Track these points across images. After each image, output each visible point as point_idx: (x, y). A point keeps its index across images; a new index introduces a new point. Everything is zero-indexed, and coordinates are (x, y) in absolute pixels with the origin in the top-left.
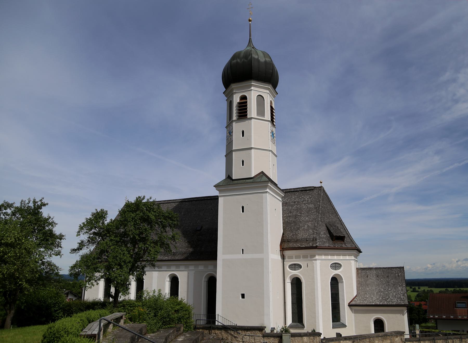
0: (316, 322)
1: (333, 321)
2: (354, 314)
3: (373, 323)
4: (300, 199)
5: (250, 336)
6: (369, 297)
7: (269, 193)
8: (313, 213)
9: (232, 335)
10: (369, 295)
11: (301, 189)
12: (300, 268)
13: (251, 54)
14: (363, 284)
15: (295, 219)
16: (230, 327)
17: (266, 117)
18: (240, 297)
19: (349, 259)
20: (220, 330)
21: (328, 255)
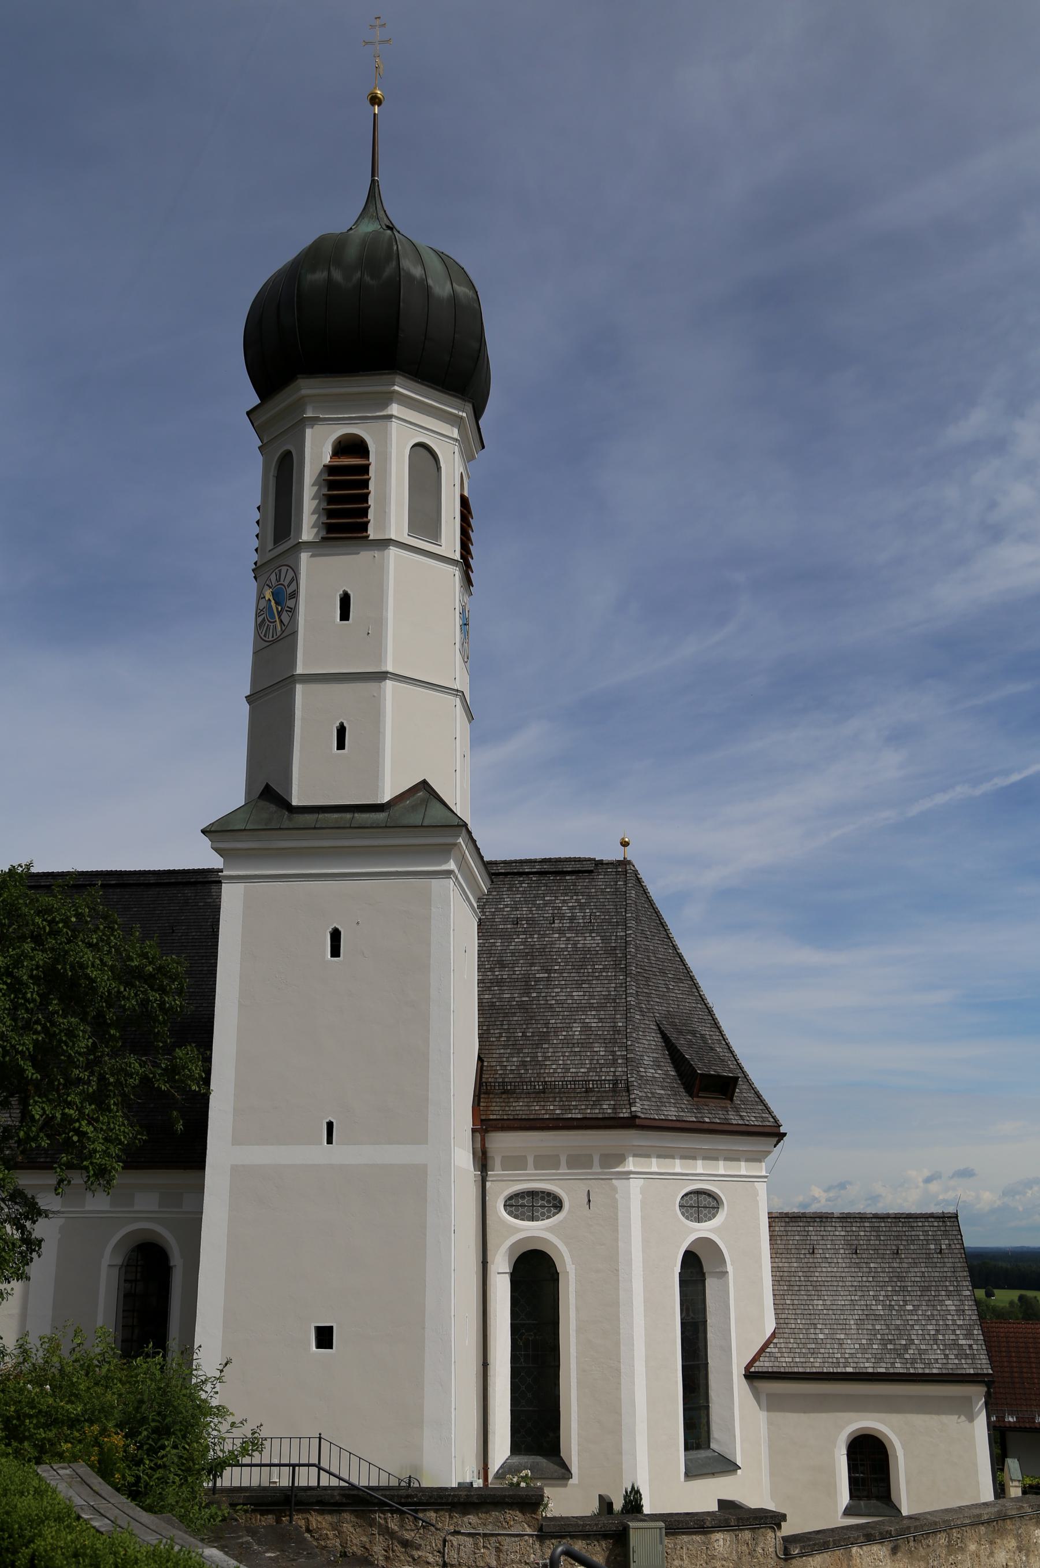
0: (621, 1453)
1: (687, 1448)
2: (766, 1413)
3: (844, 1451)
4: (538, 907)
5: (479, 1534)
6: (829, 1341)
7: (457, 878)
8: (601, 971)
9: (391, 1534)
10: (827, 1331)
11: (537, 868)
12: (553, 1210)
13: (395, 257)
14: (798, 1283)
15: (528, 994)
16: (385, 1496)
17: (443, 545)
18: (309, 1344)
19: (705, 1172)
20: (331, 1512)
21: (673, 1157)
